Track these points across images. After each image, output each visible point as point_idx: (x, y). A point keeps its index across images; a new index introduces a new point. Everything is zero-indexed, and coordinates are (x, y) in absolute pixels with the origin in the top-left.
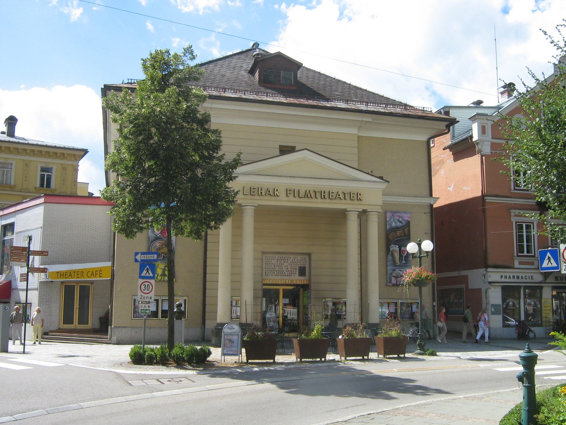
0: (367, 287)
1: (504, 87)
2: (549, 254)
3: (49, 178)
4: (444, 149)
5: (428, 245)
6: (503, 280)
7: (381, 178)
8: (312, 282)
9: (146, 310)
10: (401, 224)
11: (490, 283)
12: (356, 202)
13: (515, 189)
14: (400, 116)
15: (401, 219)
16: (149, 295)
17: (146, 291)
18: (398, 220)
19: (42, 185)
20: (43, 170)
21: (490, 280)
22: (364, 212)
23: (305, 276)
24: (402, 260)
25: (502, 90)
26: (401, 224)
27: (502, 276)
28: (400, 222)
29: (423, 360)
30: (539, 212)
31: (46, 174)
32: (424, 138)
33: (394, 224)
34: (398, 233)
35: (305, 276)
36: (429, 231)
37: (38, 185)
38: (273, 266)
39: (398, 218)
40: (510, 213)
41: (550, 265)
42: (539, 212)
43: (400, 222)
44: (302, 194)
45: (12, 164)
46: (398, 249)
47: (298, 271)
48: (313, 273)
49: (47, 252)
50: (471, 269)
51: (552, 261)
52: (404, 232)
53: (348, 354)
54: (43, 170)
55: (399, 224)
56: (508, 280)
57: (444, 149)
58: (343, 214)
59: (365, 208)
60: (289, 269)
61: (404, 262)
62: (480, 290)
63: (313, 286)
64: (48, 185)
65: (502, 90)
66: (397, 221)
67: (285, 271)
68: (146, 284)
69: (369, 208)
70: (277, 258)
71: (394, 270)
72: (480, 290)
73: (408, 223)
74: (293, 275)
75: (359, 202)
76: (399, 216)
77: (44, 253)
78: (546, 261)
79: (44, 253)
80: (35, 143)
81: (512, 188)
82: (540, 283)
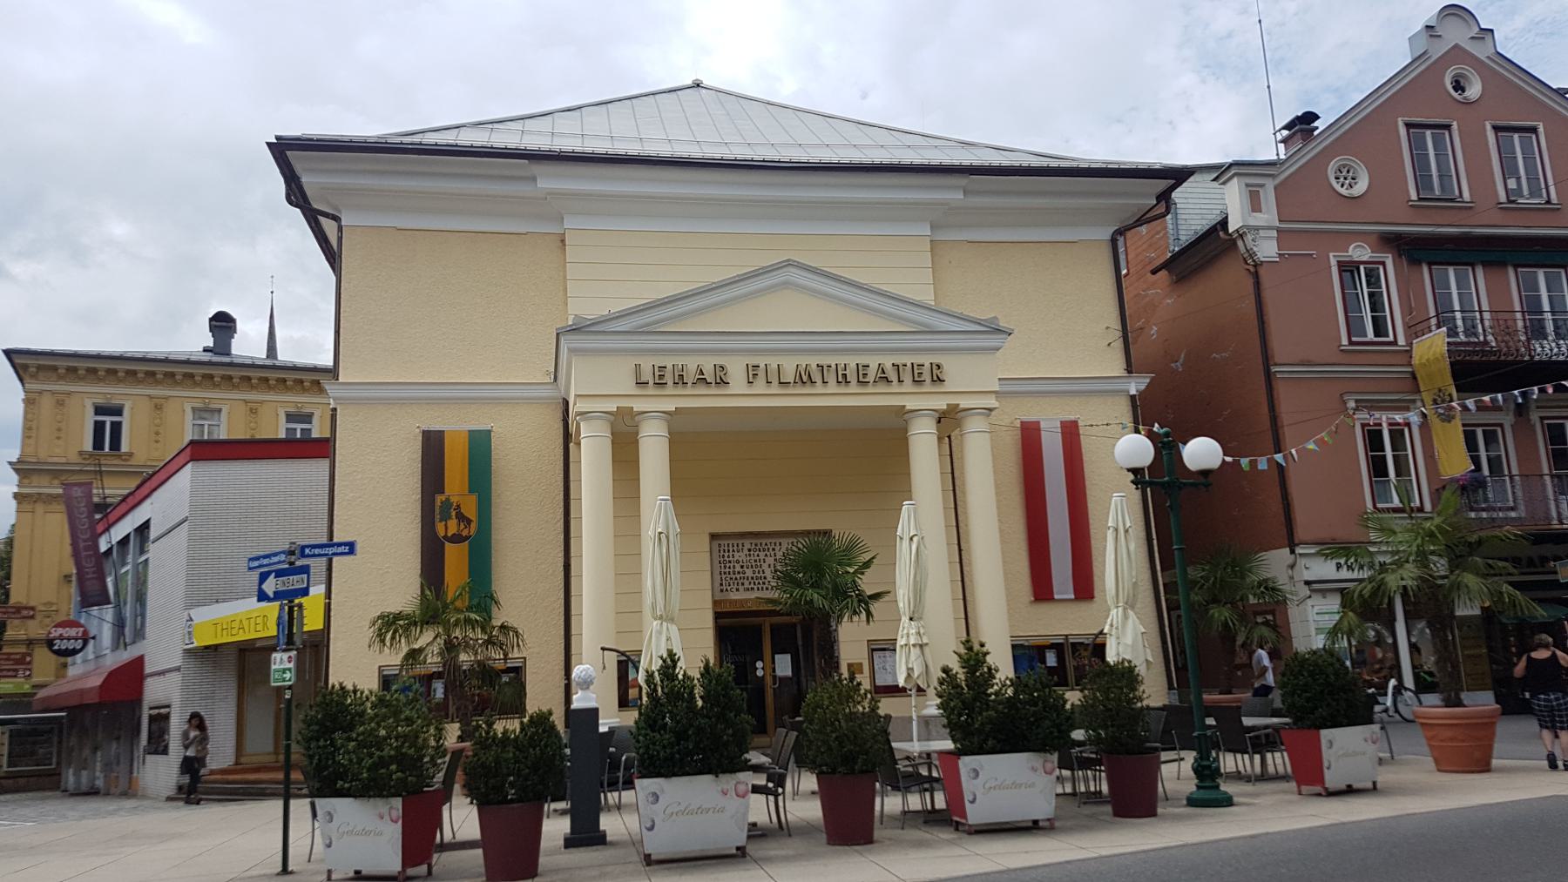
0: (962, 467)
1: (1287, 127)
3: (116, 428)
4: (1154, 272)
13: (1351, 343)
19: (98, 443)
20: (99, 410)
25: (1285, 133)
31: (108, 419)
37: (88, 445)
38: (738, 569)
40: (1345, 403)
44: (690, 377)
45: (220, 411)
54: (99, 410)
57: (1154, 272)
59: (953, 400)
64: (116, 444)
65: (1285, 133)
69: (964, 403)
70: (748, 546)
77: (25, 613)
79: (25, 613)
80: (162, 357)
81: (1345, 341)
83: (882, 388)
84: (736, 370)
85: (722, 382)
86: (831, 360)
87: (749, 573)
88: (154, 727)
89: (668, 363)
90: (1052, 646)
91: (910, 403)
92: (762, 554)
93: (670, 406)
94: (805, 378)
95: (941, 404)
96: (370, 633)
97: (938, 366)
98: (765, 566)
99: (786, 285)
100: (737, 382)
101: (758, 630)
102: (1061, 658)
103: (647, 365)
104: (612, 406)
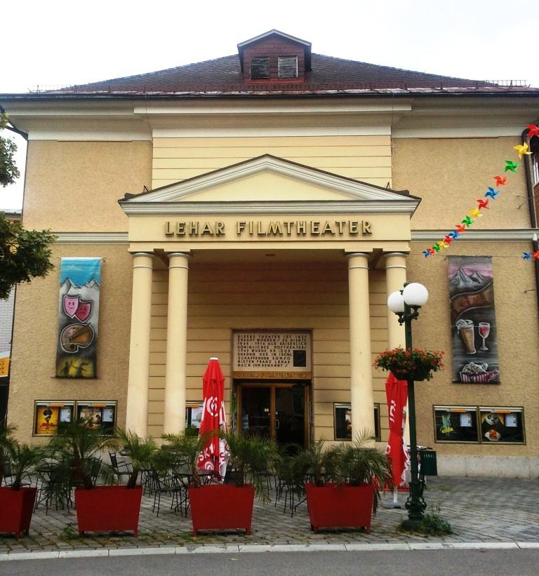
7: (405, 193)
10: (475, 284)
14: (491, 96)
15: (475, 276)
18: (470, 277)
23: (305, 366)
24: (481, 345)
26: (475, 284)
28: (475, 280)
33: (462, 284)
34: (471, 298)
35: (305, 366)
38: (250, 351)
39: (469, 274)
43: (475, 280)
46: (472, 327)
47: (292, 358)
49: (95, 376)
52: (483, 297)
53: (276, 430)
55: (471, 284)
58: (336, 266)
59: (378, 246)
60: (278, 355)
61: (486, 349)
66: (468, 279)
67: (271, 358)
69: (386, 248)
71: (466, 363)
73: (489, 283)
74: (284, 365)
76: (472, 271)
83: (327, 238)
84: (230, 224)
85: (220, 234)
86: (294, 219)
87: (257, 354)
88: (333, 87)
89: (187, 220)
90: (71, 377)
91: (348, 248)
92: (266, 343)
93: (188, 248)
94: (275, 231)
95: (369, 248)
96: (398, 524)
97: (367, 224)
98: (268, 351)
99: (266, 170)
100: (230, 234)
101: (268, 390)
102: (474, 420)
103: (174, 222)
104: (151, 248)
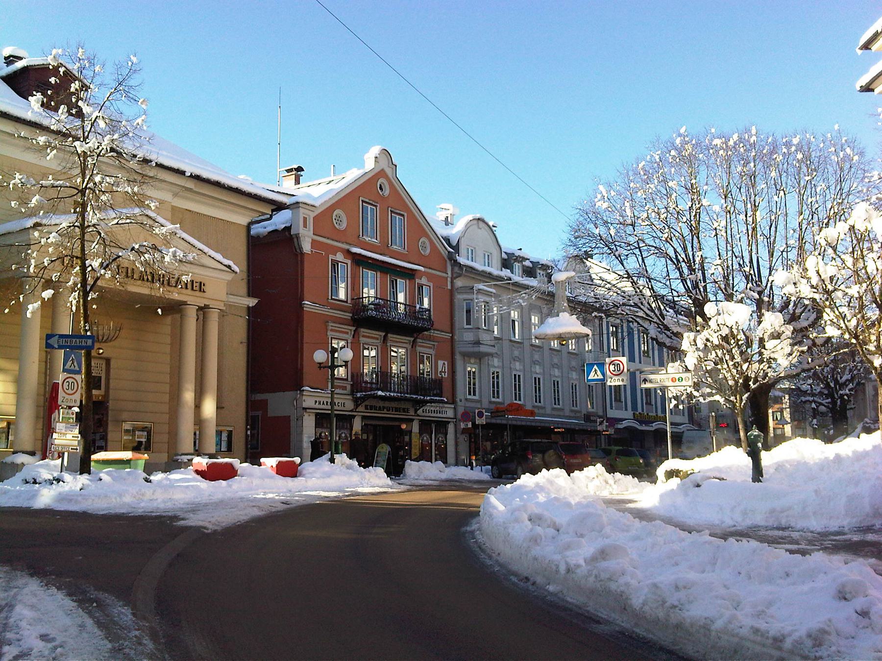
2: (595, 367)
5: (366, 353)
6: (317, 406)
8: (111, 397)
9: (69, 418)
11: (305, 409)
12: (198, 293)
16: (73, 397)
17: (70, 392)
21: (305, 405)
22: (207, 307)
27: (316, 402)
29: (381, 487)
30: (354, 328)
32: (243, 221)
36: (245, 340)
41: (596, 377)
42: (354, 328)
48: (112, 385)
50: (274, 392)
51: (599, 373)
56: (321, 406)
58: (175, 308)
62: (287, 419)
63: (111, 404)
68: (70, 380)
69: (212, 304)
72: (287, 419)
75: (201, 294)
78: (592, 373)
82: (351, 411)
